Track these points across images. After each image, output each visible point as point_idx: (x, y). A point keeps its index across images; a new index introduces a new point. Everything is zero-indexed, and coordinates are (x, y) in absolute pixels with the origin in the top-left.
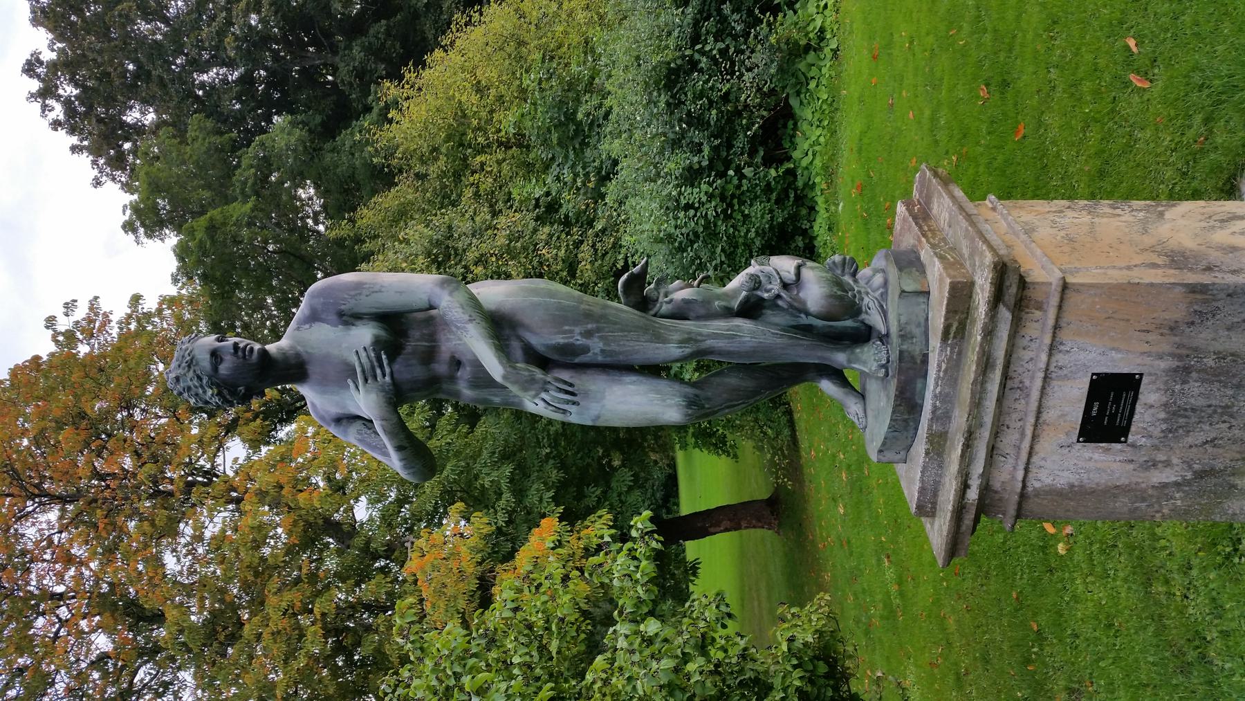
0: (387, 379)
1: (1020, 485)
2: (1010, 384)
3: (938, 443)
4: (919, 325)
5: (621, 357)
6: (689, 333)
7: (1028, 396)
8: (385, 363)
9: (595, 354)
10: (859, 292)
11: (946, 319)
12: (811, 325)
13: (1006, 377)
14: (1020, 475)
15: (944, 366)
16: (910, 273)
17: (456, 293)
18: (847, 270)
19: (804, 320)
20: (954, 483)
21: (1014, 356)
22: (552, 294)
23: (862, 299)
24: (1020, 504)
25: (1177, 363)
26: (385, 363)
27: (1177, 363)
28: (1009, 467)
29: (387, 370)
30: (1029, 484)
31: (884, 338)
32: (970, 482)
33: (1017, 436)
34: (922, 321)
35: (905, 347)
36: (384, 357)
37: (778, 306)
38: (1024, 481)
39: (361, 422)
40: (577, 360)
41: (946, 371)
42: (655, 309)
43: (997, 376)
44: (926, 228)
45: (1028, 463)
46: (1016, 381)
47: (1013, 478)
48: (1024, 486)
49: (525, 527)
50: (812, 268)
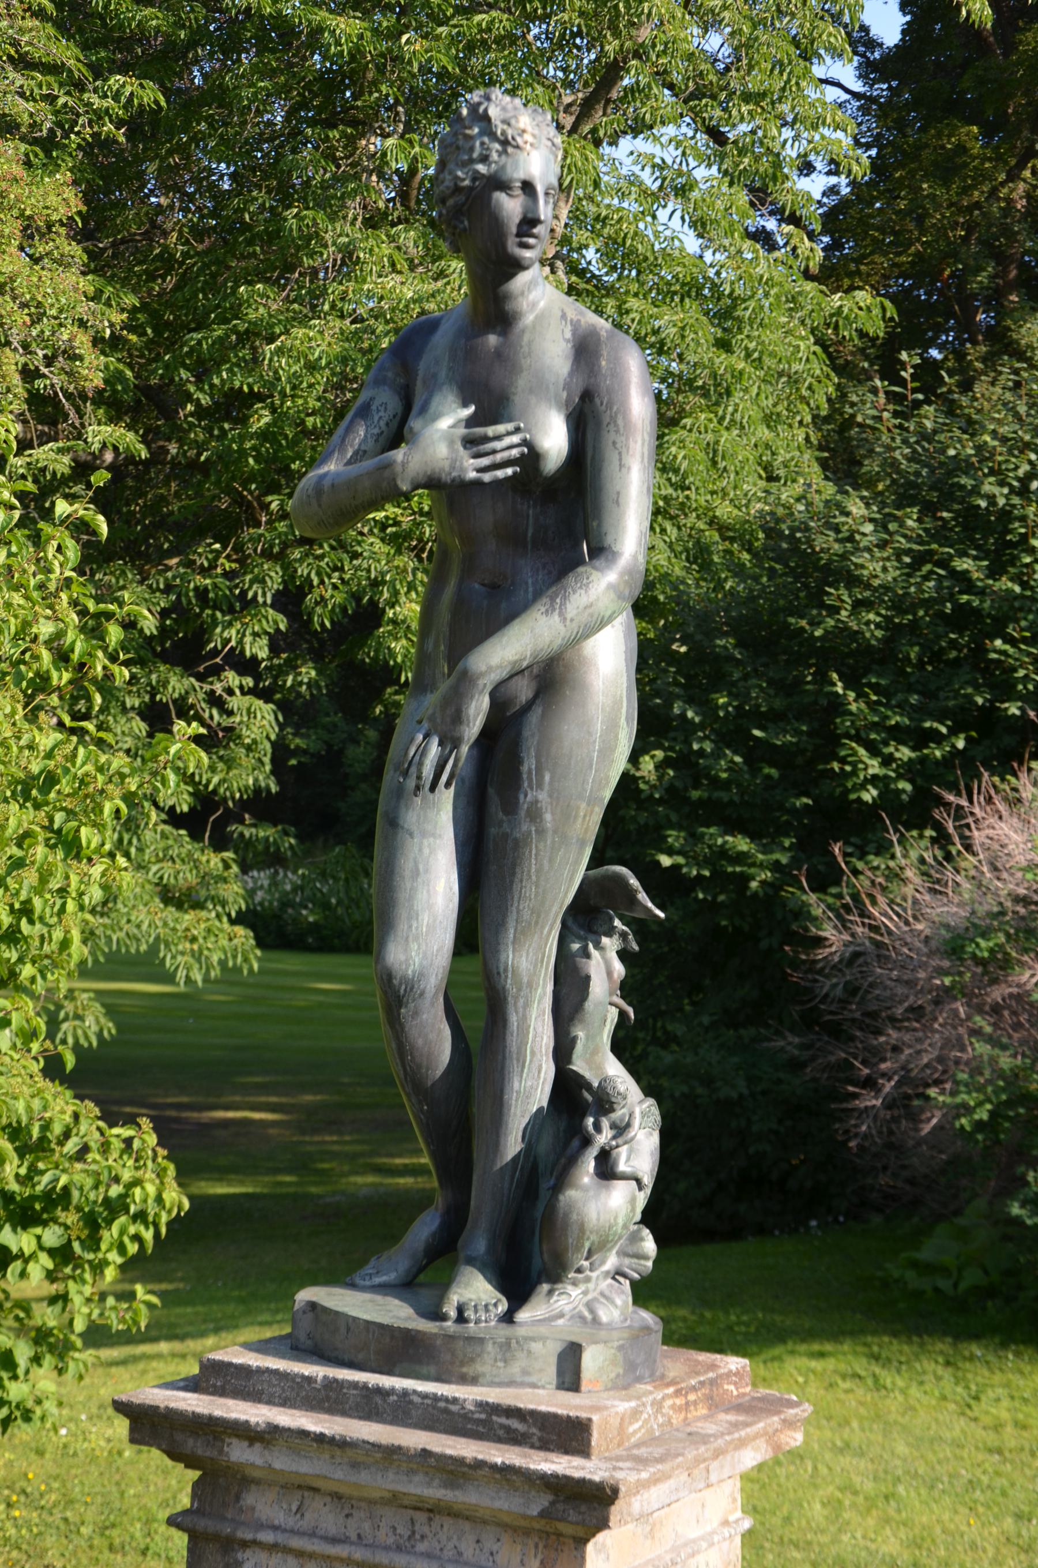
0: (472, 475)
1: (249, 1536)
2: (421, 1517)
3: (328, 1398)
4: (525, 1372)
5: (493, 868)
6: (530, 985)
7: (399, 1549)
8: (500, 474)
9: (500, 824)
10: (588, 1280)
11: (533, 1413)
12: (536, 1197)
13: (433, 1510)
14: (267, 1537)
15: (454, 1408)
16: (613, 1363)
17: (613, 596)
18: (627, 1261)
19: (545, 1184)
20: (261, 1420)
21: (467, 1526)
22: (607, 750)
23: (575, 1284)
24: (216, 1537)
25: (464, 1370)
26: (500, 474)
27: (464, 1370)
28: (280, 1518)
29: (487, 477)
30: (248, 1553)
31: (508, 1318)
32: (258, 1446)
33: (333, 1531)
34: (533, 1379)
35: (490, 1347)
36: (509, 471)
37: (573, 1136)
38: (255, 1543)
39: (400, 410)
40: (491, 791)
41: (446, 1411)
42: (575, 928)
43: (436, 1493)
44: (692, 1397)
45: (287, 1550)
46: (426, 1529)
47: (261, 1526)
48: (245, 1544)
49: (663, 1313)
50: (633, 1201)
